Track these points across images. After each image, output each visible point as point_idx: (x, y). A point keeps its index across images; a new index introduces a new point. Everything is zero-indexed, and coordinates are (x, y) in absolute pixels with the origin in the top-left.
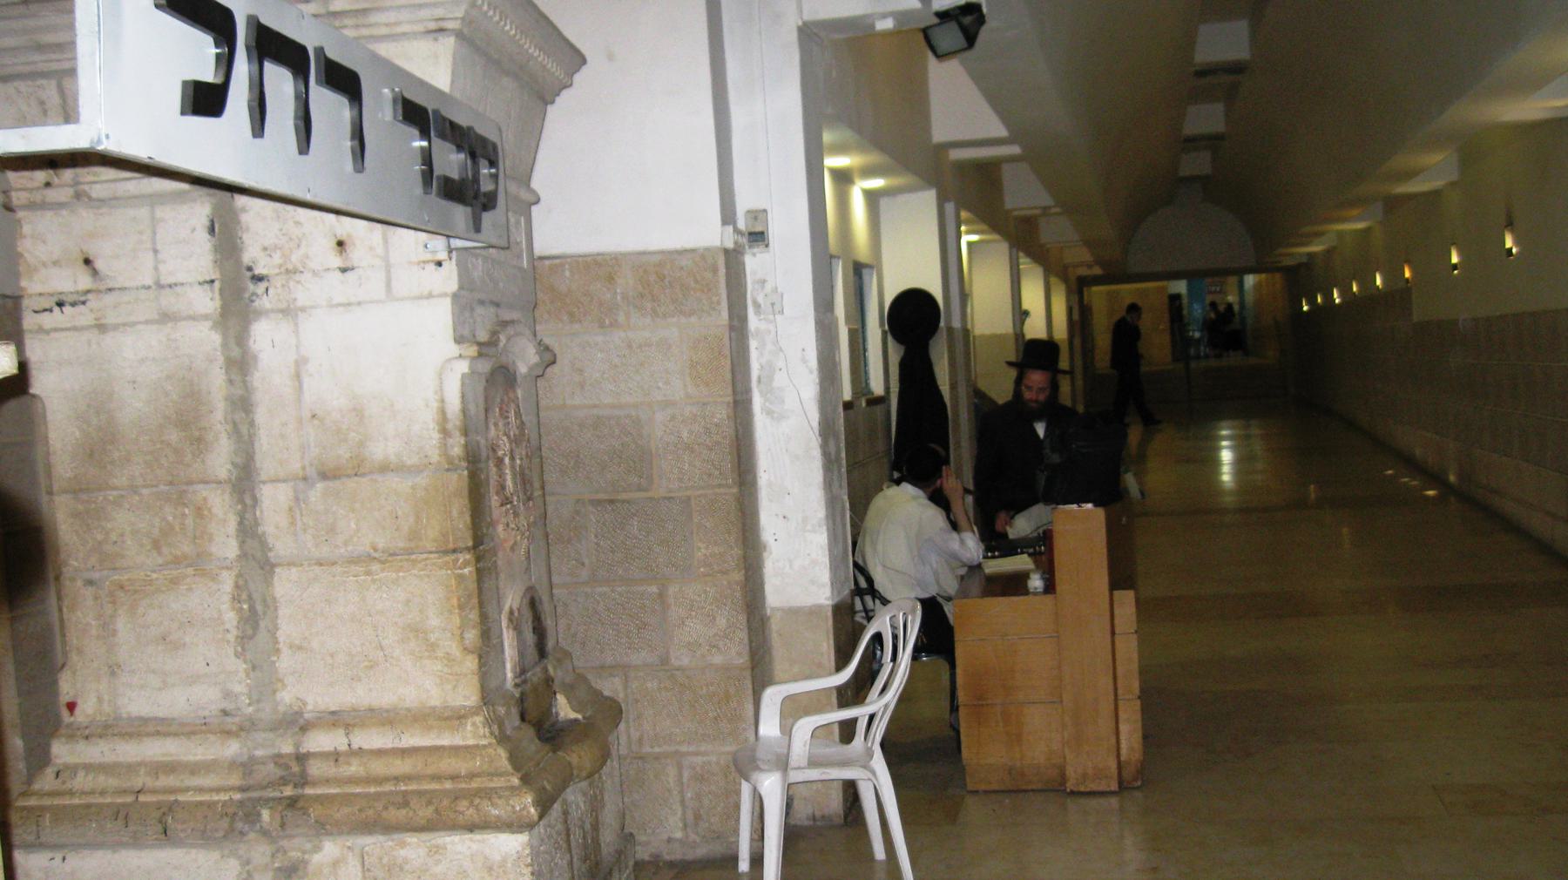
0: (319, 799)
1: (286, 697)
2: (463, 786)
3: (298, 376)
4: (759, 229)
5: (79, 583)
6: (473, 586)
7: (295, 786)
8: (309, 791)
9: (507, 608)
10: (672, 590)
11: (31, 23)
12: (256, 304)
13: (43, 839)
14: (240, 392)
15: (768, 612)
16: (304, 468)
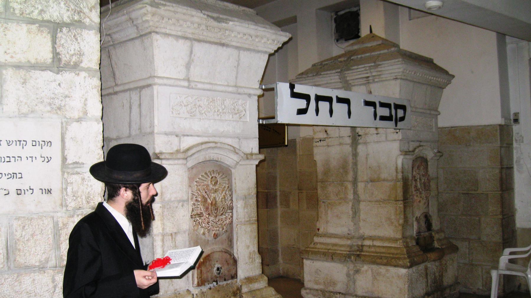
0: (365, 256)
1: (361, 232)
2: (394, 256)
3: (367, 158)
4: (516, 118)
5: (321, 202)
6: (402, 209)
7: (360, 252)
8: (362, 253)
9: (416, 216)
10: (483, 219)
11: (314, 80)
12: (359, 141)
13: (309, 257)
14: (355, 161)
15: (516, 229)
16: (367, 179)
